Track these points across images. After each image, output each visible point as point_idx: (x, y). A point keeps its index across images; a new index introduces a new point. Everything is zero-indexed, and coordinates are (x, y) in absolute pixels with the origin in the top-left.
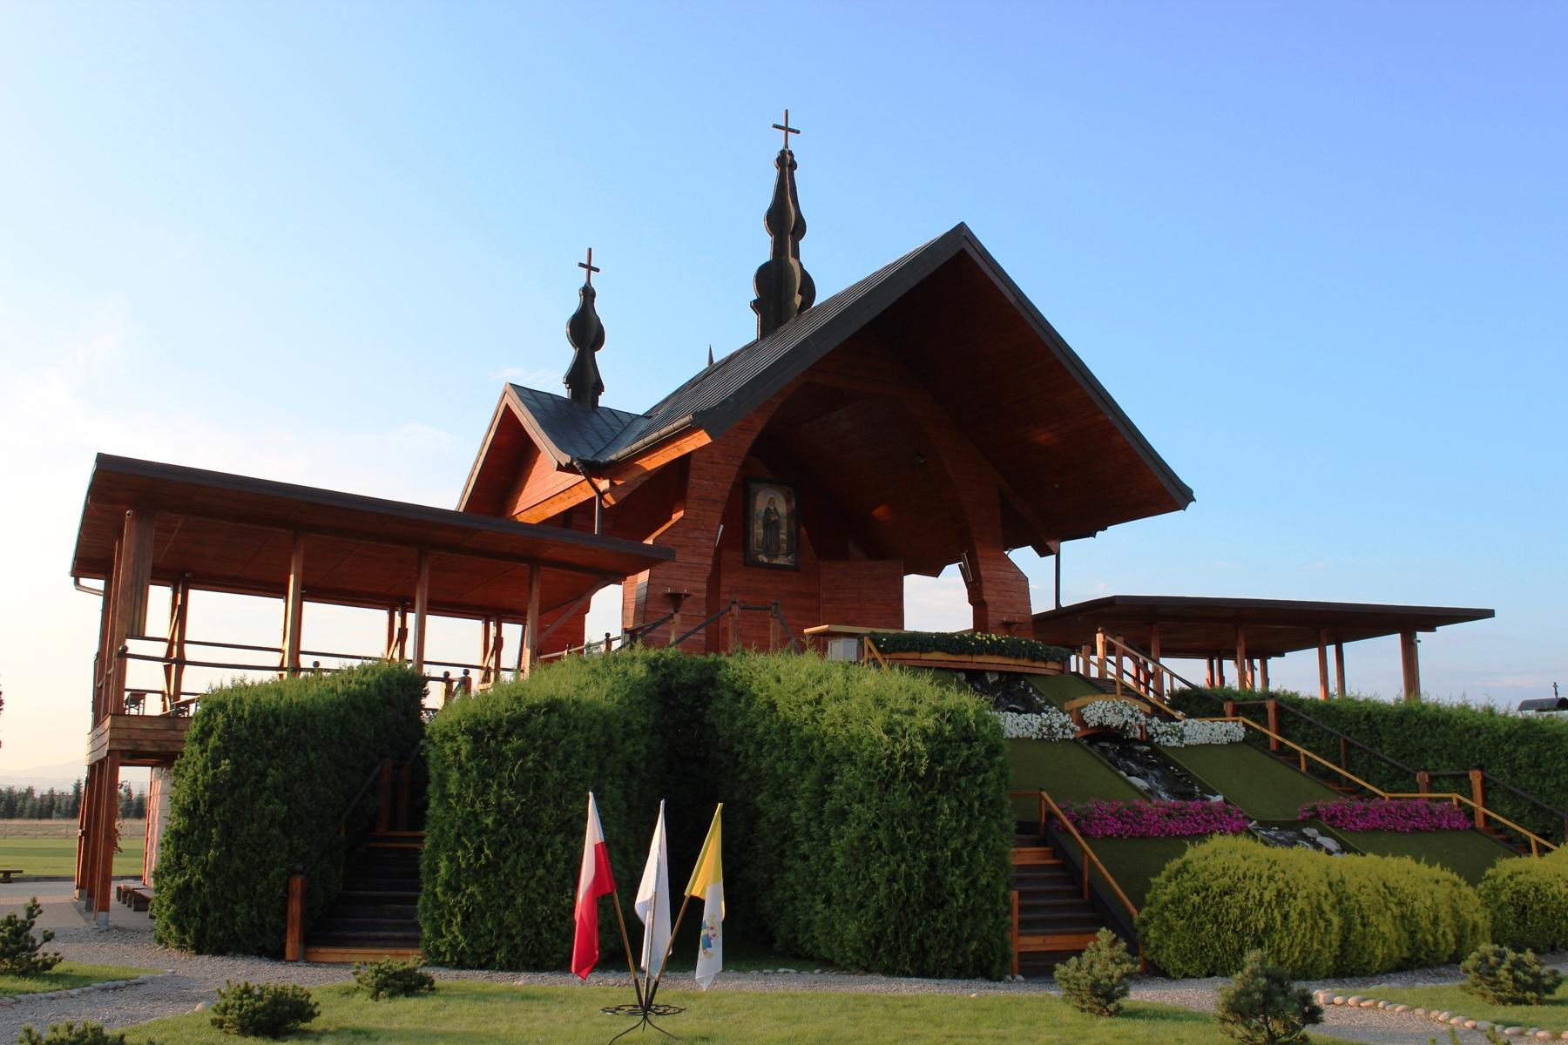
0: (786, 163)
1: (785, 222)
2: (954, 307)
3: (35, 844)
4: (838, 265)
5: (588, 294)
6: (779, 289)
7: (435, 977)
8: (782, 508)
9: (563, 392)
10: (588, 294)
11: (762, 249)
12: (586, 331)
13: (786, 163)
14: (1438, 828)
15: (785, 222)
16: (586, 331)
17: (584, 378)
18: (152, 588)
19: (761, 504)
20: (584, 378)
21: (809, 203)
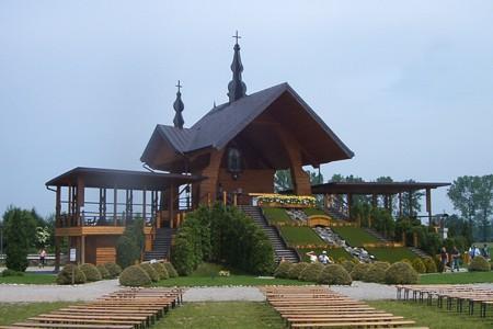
0: (237, 48)
1: (237, 67)
2: (286, 110)
3: (350, 324)
4: (255, 84)
5: (179, 94)
6: (237, 89)
7: (114, 262)
8: (237, 154)
9: (173, 125)
10: (179, 94)
11: (230, 76)
12: (179, 106)
13: (237, 48)
14: (297, 278)
15: (237, 67)
16: (179, 106)
17: (179, 121)
18: (86, 189)
19: (231, 154)
20: (179, 121)
21: (244, 61)
